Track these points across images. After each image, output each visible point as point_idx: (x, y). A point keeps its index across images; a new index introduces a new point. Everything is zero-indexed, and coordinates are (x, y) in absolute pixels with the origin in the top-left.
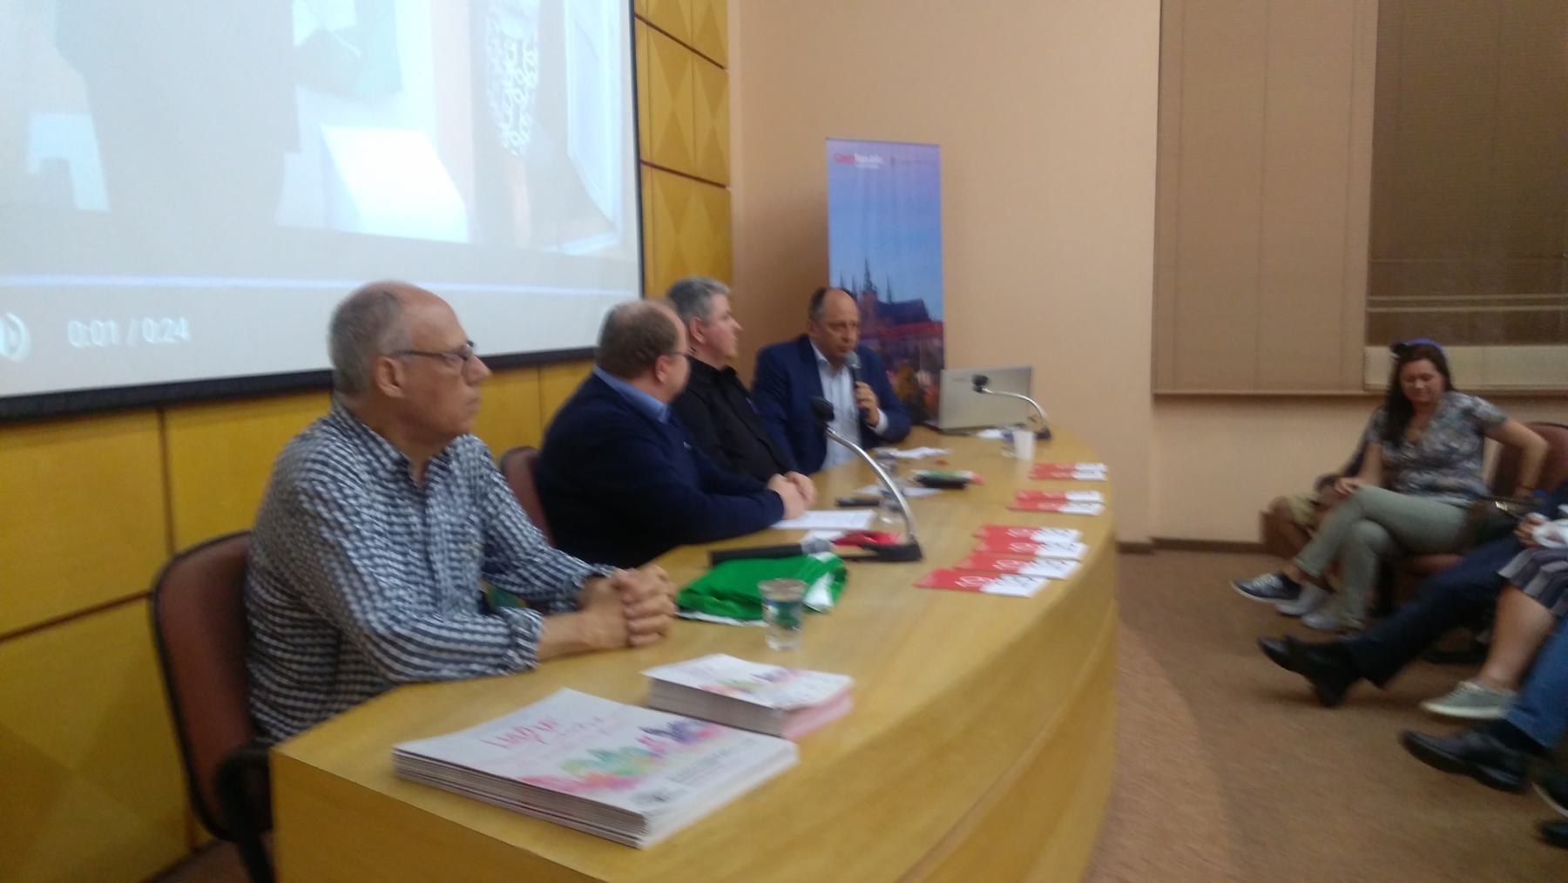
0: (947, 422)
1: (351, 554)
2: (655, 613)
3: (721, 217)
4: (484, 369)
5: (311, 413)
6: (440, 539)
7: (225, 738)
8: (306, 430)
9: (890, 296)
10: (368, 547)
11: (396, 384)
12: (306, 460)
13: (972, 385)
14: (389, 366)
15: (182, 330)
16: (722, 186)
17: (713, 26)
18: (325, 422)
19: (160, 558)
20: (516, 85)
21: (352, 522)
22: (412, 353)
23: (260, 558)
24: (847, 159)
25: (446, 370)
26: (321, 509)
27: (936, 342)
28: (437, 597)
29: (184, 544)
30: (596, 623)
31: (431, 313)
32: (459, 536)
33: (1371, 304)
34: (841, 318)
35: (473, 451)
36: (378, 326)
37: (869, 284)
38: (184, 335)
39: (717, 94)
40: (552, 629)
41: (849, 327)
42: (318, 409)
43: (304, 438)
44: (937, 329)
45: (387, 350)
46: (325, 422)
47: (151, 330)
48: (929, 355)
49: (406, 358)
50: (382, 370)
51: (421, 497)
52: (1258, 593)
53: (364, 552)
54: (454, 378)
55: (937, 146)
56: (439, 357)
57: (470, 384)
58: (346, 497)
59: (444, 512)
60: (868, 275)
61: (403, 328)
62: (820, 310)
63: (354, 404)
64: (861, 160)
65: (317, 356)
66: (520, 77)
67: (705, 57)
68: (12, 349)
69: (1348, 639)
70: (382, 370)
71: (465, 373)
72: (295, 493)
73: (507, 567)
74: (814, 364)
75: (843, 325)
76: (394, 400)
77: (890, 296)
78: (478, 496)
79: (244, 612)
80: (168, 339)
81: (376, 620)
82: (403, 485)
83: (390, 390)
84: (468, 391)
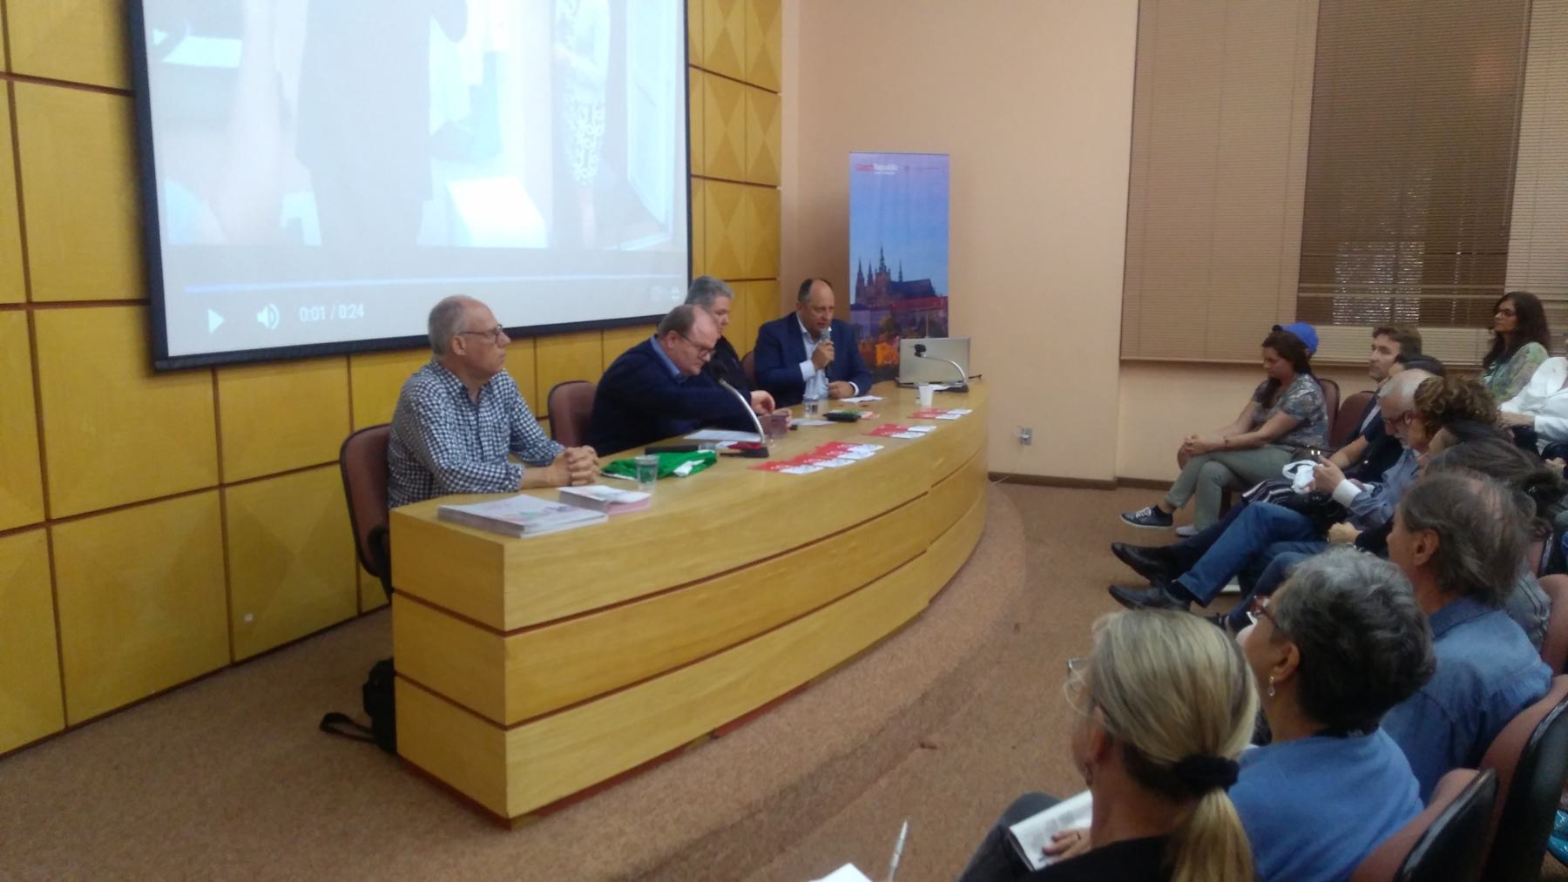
0: (903, 380)
1: (434, 432)
2: (586, 469)
3: (771, 213)
4: (507, 339)
5: (419, 362)
6: (487, 430)
7: (371, 520)
8: (417, 371)
9: (901, 277)
10: (442, 429)
12: (416, 386)
13: (914, 351)
14: (458, 340)
15: (360, 311)
16: (774, 187)
18: (427, 367)
19: (346, 434)
20: (586, 136)
21: (435, 417)
22: (470, 333)
23: (394, 436)
24: (867, 168)
25: (485, 341)
26: (421, 410)
27: (941, 314)
28: (483, 459)
29: (357, 428)
30: (551, 473)
31: (478, 313)
32: (497, 428)
33: (1300, 290)
34: (821, 304)
35: (508, 384)
36: (451, 320)
37: (883, 267)
38: (362, 314)
39: (770, 117)
40: (529, 474)
41: (827, 310)
42: (425, 359)
43: (416, 375)
44: (943, 303)
46: (427, 367)
47: (343, 312)
48: (932, 323)
49: (466, 335)
50: (455, 342)
51: (476, 409)
52: (1137, 521)
53: (440, 431)
54: (492, 345)
55: (947, 155)
56: (483, 334)
57: (499, 347)
58: (433, 405)
59: (489, 415)
60: (882, 259)
61: (465, 320)
62: (807, 297)
63: (442, 359)
64: (879, 168)
66: (590, 130)
67: (758, 87)
68: (271, 323)
69: (818, 469)
70: (455, 342)
71: (496, 341)
72: (410, 402)
73: (523, 448)
74: (799, 336)
75: (824, 308)
76: (461, 357)
77: (901, 277)
78: (509, 409)
79: (386, 464)
80: (352, 316)
82: (466, 400)
83: (459, 352)
84: (499, 351)
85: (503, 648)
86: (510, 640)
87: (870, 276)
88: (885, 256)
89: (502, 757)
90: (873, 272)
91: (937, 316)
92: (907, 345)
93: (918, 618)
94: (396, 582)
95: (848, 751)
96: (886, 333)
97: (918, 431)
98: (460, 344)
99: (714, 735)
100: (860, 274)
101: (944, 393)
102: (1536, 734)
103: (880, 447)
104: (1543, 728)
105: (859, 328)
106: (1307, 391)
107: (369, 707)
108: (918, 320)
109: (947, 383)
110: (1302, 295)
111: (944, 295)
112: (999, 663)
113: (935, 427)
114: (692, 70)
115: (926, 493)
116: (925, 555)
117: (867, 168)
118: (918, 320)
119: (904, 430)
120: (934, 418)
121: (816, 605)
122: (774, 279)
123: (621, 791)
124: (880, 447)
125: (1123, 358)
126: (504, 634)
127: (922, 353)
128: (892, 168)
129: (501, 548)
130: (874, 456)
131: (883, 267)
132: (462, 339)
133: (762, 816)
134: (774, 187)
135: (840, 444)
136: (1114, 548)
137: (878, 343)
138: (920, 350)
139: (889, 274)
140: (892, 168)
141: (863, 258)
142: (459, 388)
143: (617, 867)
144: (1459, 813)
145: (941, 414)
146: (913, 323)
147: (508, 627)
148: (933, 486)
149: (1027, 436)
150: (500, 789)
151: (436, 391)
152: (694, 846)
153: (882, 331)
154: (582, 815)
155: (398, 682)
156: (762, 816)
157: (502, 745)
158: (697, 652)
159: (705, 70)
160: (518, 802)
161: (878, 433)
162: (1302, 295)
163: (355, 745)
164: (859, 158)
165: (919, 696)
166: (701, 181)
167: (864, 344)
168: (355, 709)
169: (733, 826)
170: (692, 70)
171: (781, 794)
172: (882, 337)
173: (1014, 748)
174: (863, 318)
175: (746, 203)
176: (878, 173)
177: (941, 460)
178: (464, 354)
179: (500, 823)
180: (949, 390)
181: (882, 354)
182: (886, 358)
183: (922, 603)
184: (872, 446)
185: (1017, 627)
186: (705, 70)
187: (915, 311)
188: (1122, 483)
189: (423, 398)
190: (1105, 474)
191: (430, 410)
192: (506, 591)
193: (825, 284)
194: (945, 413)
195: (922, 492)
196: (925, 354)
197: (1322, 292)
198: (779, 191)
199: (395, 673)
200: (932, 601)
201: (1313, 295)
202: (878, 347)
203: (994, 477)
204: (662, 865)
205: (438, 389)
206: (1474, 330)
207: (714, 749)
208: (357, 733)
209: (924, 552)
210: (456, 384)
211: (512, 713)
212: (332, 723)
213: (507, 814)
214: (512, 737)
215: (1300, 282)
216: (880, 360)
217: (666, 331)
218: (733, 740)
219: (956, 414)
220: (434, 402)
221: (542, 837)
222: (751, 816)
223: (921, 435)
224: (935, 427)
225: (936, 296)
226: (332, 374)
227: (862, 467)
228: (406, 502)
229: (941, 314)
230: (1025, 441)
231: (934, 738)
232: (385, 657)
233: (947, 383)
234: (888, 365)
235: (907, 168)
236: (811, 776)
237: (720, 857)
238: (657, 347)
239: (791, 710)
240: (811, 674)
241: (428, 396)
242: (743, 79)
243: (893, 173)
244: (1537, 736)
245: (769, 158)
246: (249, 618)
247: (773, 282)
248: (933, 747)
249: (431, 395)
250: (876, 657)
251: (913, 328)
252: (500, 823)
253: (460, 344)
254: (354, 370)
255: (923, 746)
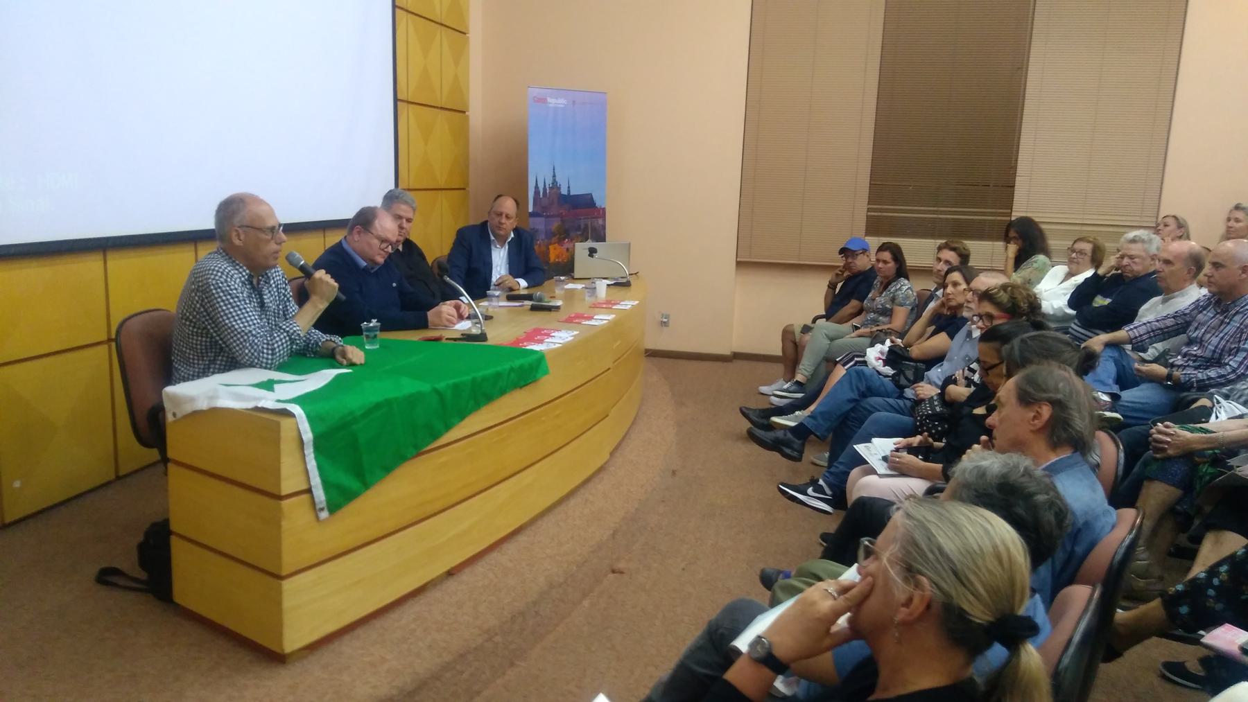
3: (461, 133)
9: (569, 191)
11: (240, 240)
14: (237, 231)
17: (459, 9)
24: (542, 100)
25: (263, 236)
27: (600, 221)
33: (869, 210)
35: (279, 276)
37: (555, 182)
39: (460, 53)
42: (213, 246)
44: (602, 213)
45: (238, 224)
48: (594, 229)
49: (245, 229)
50: (234, 234)
56: (260, 229)
58: (231, 290)
60: (554, 176)
64: (552, 101)
65: (209, 223)
70: (234, 234)
77: (569, 191)
81: (238, 325)
83: (237, 242)
85: (280, 509)
86: (285, 503)
87: (545, 189)
88: (556, 175)
89: (279, 603)
90: (547, 186)
91: (598, 223)
92: (581, 248)
93: (601, 469)
94: (171, 454)
95: (561, 580)
96: (557, 236)
97: (602, 319)
98: (238, 235)
99: (450, 573)
100: (537, 187)
101: (611, 286)
102: (1116, 556)
103: (576, 333)
104: (1122, 551)
105: (534, 232)
106: (907, 287)
107: (144, 562)
108: (582, 227)
109: (614, 279)
110: (869, 213)
111: (603, 207)
112: (663, 501)
113: (614, 316)
114: (398, 11)
115: (609, 369)
116: (607, 418)
117: (542, 100)
118: (582, 227)
119: (590, 318)
120: (611, 308)
121: (529, 463)
122: (464, 189)
123: (378, 623)
124: (576, 333)
125: (738, 260)
126: (280, 498)
127: (594, 254)
128: (562, 102)
129: (278, 424)
130: (573, 340)
131: (555, 182)
132: (240, 231)
133: (498, 639)
134: (464, 112)
135: (543, 330)
136: (741, 410)
137: (551, 244)
138: (592, 252)
139: (559, 188)
140: (562, 102)
141: (539, 174)
142: (247, 274)
143: (384, 691)
144: (1088, 624)
145: (615, 304)
146: (578, 228)
147: (284, 493)
148: (614, 362)
149: (665, 320)
150: (277, 629)
151: (232, 276)
152: (446, 667)
153: (554, 235)
154: (347, 646)
155: (174, 541)
156: (498, 639)
157: (279, 592)
158: (438, 506)
159: (407, 11)
160: (293, 640)
161: (571, 321)
162: (869, 213)
163: (131, 596)
164: (534, 92)
165: (611, 532)
166: (405, 104)
167: (540, 245)
168: (128, 562)
169: (475, 649)
170: (398, 11)
171: (512, 618)
172: (554, 239)
173: (683, 569)
174: (539, 224)
175: (441, 122)
176: (551, 105)
177: (618, 343)
178: (242, 244)
179: (274, 658)
180: (616, 284)
181: (555, 253)
182: (558, 257)
183: (606, 456)
184: (569, 332)
185: (674, 472)
186: (407, 11)
187: (580, 219)
188: (737, 356)
189: (222, 283)
190: (726, 351)
191: (230, 294)
192: (282, 461)
193: (500, 199)
194: (619, 304)
195: (607, 368)
196: (596, 256)
197: (941, 214)
198: (468, 116)
199: (170, 533)
200: (612, 454)
201: (879, 214)
202: (551, 247)
203: (652, 354)
204: (422, 685)
205: (233, 275)
206: (990, 243)
207: (452, 584)
208: (134, 585)
209: (607, 416)
210: (244, 271)
211: (289, 561)
212: (107, 577)
213: (283, 650)
214: (287, 585)
215: (869, 204)
216: (552, 258)
217: (352, 229)
218: (466, 576)
219: (627, 305)
220: (232, 287)
221: (314, 669)
222: (489, 639)
223: (605, 322)
224: (614, 316)
225: (597, 207)
226: (91, 265)
227: (566, 349)
228: (191, 377)
229: (600, 221)
230: (664, 324)
231: (621, 565)
232: (159, 519)
233: (614, 279)
234: (558, 263)
235: (574, 102)
236: (535, 603)
237: (465, 676)
238: (345, 246)
239: (511, 548)
240: (524, 519)
241: (226, 281)
242: (439, 21)
243: (562, 106)
244: (1118, 557)
245: (459, 89)
246: (17, 484)
247: (462, 191)
248: (622, 573)
249: (229, 280)
250: (572, 502)
251: (579, 233)
252: (274, 658)
253: (238, 235)
254: (110, 263)
255: (613, 572)
